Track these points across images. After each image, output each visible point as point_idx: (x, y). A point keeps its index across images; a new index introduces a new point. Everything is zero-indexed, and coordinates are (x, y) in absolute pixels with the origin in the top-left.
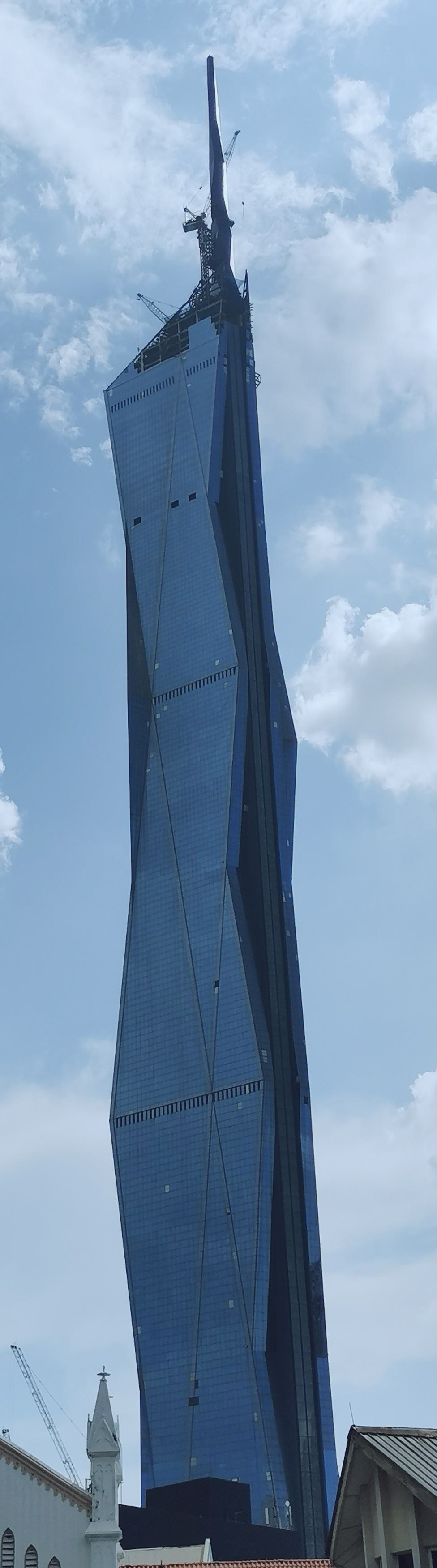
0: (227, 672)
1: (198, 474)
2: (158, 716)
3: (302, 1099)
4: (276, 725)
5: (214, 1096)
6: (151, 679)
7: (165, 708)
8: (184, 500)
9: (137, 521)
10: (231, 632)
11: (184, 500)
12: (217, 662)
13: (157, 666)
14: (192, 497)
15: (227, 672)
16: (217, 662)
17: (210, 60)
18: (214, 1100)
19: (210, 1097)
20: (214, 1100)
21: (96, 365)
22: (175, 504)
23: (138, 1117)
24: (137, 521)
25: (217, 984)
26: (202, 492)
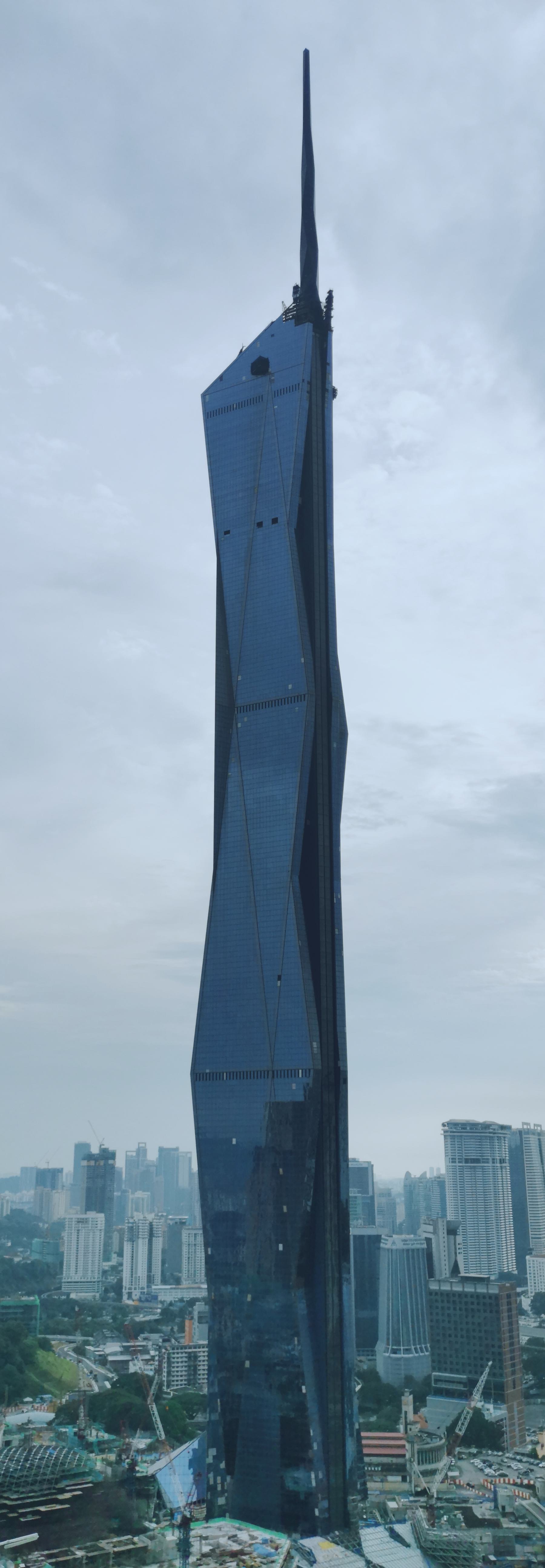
0: (299, 698)
1: (283, 505)
2: (239, 725)
3: (342, 1081)
4: (335, 745)
5: (274, 1074)
6: (235, 689)
7: (246, 719)
8: (267, 523)
9: (227, 532)
10: (303, 660)
11: (267, 523)
12: (290, 687)
13: (240, 678)
14: (275, 521)
15: (299, 698)
16: (290, 687)
17: (306, 54)
18: (273, 1077)
19: (271, 1073)
20: (273, 1077)
21: (346, 1369)
22: (260, 525)
23: (215, 1076)
24: (227, 532)
25: (279, 978)
26: (283, 519)
